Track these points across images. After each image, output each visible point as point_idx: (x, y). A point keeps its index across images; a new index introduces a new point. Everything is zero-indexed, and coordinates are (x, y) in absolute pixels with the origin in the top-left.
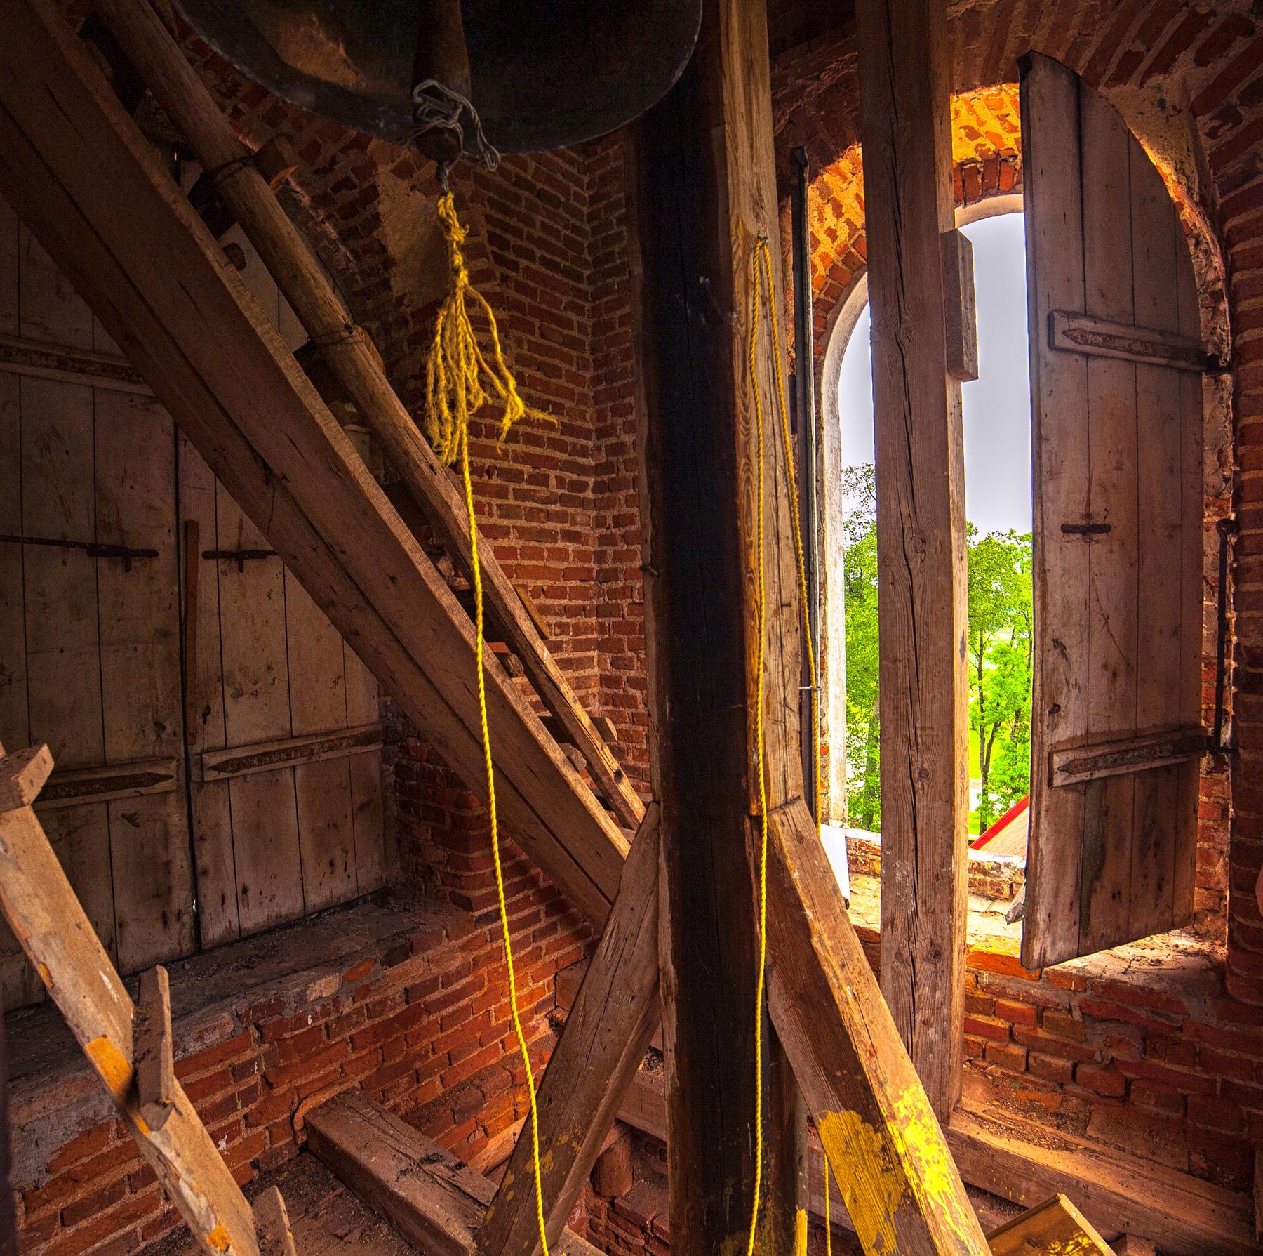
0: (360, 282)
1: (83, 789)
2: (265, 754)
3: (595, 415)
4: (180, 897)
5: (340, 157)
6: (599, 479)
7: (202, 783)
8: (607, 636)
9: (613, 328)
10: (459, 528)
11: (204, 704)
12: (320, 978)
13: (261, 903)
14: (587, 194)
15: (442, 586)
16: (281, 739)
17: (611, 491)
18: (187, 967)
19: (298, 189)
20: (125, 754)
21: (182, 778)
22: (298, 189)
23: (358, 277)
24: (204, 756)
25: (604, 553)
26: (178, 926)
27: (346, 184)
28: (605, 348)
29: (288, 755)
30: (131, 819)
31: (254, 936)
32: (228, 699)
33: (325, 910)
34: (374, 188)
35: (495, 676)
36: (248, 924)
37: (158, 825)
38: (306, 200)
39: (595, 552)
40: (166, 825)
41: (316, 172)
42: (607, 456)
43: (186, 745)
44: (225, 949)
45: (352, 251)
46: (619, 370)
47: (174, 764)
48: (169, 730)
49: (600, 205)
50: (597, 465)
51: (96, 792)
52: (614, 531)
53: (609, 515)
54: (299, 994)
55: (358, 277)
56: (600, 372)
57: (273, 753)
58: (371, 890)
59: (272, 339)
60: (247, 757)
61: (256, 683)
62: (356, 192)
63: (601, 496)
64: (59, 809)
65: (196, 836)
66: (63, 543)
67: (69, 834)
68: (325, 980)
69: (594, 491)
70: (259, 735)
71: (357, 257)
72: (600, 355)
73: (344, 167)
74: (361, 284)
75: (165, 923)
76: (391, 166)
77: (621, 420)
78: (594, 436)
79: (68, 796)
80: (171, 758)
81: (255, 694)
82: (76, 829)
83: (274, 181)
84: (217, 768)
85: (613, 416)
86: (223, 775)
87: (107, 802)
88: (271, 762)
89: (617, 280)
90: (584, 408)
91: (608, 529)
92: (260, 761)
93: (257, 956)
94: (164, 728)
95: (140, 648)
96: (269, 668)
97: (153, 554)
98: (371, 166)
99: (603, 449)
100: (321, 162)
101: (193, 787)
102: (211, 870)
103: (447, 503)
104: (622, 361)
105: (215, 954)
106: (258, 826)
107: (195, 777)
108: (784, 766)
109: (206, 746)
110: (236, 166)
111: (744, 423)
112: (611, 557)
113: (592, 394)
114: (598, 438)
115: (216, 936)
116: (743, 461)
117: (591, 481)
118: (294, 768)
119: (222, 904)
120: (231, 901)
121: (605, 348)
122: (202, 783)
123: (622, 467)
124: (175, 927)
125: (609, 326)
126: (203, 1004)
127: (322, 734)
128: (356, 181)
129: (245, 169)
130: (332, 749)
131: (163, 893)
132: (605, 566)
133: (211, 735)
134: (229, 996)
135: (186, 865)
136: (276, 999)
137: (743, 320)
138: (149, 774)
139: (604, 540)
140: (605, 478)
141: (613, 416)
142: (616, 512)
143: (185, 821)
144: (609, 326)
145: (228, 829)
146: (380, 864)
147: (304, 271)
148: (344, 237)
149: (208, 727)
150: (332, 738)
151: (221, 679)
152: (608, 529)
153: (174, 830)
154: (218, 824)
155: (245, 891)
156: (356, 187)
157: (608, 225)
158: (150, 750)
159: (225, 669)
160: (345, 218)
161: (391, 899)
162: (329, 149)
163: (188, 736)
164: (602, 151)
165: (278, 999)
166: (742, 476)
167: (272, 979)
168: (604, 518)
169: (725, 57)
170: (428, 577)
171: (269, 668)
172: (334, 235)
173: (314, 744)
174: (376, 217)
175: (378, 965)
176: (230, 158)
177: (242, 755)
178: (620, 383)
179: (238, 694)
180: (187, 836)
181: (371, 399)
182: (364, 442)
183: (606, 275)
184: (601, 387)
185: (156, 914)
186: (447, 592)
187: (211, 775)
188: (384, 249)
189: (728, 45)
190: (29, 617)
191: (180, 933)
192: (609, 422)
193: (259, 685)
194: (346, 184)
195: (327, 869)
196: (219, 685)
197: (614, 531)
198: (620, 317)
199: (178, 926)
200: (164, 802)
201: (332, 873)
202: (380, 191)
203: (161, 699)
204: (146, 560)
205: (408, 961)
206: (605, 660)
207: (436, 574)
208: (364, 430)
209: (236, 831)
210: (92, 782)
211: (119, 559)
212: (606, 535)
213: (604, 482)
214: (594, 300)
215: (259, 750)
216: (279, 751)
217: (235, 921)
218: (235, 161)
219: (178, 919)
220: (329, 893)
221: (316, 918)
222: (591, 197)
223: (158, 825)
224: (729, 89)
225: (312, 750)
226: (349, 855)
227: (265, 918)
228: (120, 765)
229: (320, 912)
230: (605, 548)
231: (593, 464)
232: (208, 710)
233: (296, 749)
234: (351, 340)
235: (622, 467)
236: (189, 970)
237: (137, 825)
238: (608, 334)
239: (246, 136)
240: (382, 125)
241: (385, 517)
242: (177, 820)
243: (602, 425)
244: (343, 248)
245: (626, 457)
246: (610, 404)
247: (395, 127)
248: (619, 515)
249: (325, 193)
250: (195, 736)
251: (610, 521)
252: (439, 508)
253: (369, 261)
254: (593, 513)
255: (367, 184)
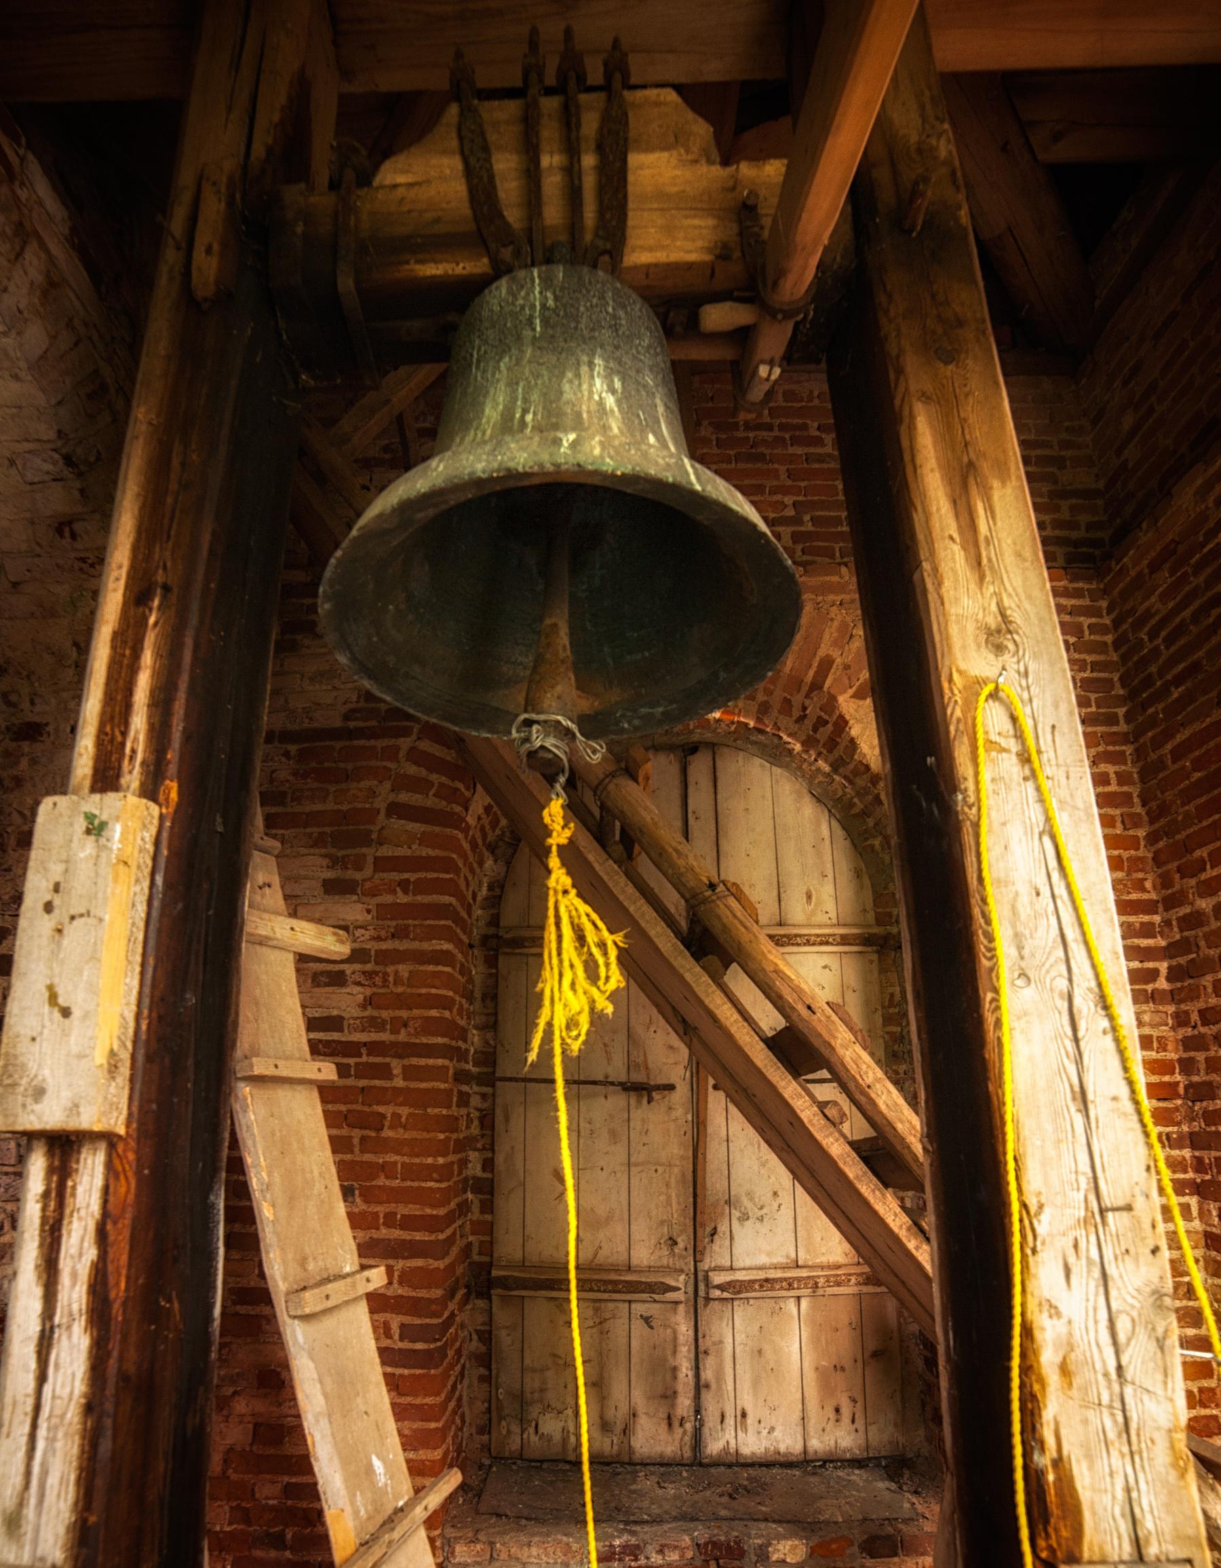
0: (859, 803)
1: (610, 1287)
2: (767, 1280)
3: (1159, 881)
4: (684, 1404)
5: (807, 702)
6: (1174, 963)
7: (708, 1299)
8: (1208, 1177)
9: (1165, 767)
10: (847, 1070)
11: (713, 1225)
12: (785, 1538)
13: (759, 1433)
14: (1107, 621)
15: (831, 1134)
16: (784, 1268)
17: (1192, 977)
18: (685, 1474)
19: (789, 740)
20: (645, 1263)
21: (691, 1289)
22: (789, 740)
23: (856, 800)
24: (710, 1274)
25: (1191, 1061)
26: (680, 1431)
27: (821, 722)
28: (1159, 795)
29: (790, 1285)
30: (647, 1320)
31: (752, 1465)
32: (735, 1223)
33: (831, 1461)
34: (841, 717)
35: (904, 1240)
36: (746, 1451)
37: (669, 1331)
38: (798, 747)
39: (1180, 1060)
40: (675, 1332)
41: (797, 721)
42: (1181, 931)
43: (695, 1262)
44: (723, 1468)
45: (845, 777)
46: (1180, 818)
47: (682, 1277)
48: (681, 1245)
49: (1125, 626)
50: (1170, 945)
51: (619, 1292)
52: (1203, 1030)
53: (1193, 1009)
54: (760, 1546)
55: (856, 800)
56: (1156, 826)
57: (775, 1280)
58: (883, 1453)
59: (643, 914)
60: (750, 1281)
61: (761, 1208)
62: (830, 727)
63: (1179, 985)
64: (595, 1301)
65: (702, 1348)
66: (606, 1083)
67: (601, 1323)
68: (790, 1543)
69: (1168, 979)
70: (763, 1260)
71: (851, 782)
72: (1154, 805)
73: (813, 711)
74: (859, 806)
75: (670, 1425)
76: (851, 692)
77: (1193, 882)
78: (1161, 908)
79: (599, 1291)
80: (682, 1271)
81: (761, 1219)
82: (606, 1320)
83: (640, 779)
84: (721, 1287)
85: (1182, 878)
86: (726, 1295)
87: (630, 1302)
88: (772, 1289)
89: (1161, 706)
90: (1140, 875)
91: (1194, 1027)
92: (761, 1286)
93: (745, 1488)
94: (676, 1243)
95: (660, 1169)
96: (775, 1194)
97: (671, 1087)
98: (833, 699)
99: (1174, 923)
100: (796, 713)
101: (701, 1302)
102: (713, 1385)
103: (830, 1045)
104: (1183, 804)
105: (713, 1470)
106: (760, 1352)
107: (702, 1293)
108: (1128, 1490)
109: (713, 1265)
110: (607, 780)
111: (985, 942)
112: (1202, 1066)
113: (1150, 855)
114: (1166, 910)
115: (715, 1452)
116: (989, 996)
117: (1163, 966)
118: (799, 1298)
119: (722, 1422)
120: (730, 1421)
121: (1159, 795)
122: (708, 1299)
123: (1202, 943)
124: (678, 1431)
125: (1160, 765)
126: (675, 1519)
127: (830, 1267)
128: (826, 717)
129: (615, 781)
130: (838, 1284)
131: (669, 1396)
132: (1196, 1079)
133: (718, 1255)
134: (697, 1520)
135: (690, 1374)
136: (735, 1542)
137: (972, 799)
138: (662, 1283)
139: (1188, 1043)
140: (1182, 960)
141: (1182, 878)
142: (1201, 1005)
143: (691, 1333)
144: (1160, 765)
145: (729, 1349)
146: (896, 1425)
147: (667, 847)
148: (835, 767)
149: (716, 1247)
150: (839, 1272)
151: (728, 1202)
152: (1194, 1027)
153: (681, 1339)
154: (721, 1342)
155: (744, 1415)
156: (827, 722)
157: (1140, 644)
158: (665, 1261)
159: (732, 1193)
160: (830, 751)
161: (907, 1474)
162: (797, 699)
163: (697, 1252)
164: (1117, 564)
165: (737, 1543)
166: (990, 1019)
167: (741, 1519)
168: (1187, 1013)
169: (912, 486)
170: (813, 1125)
171: (775, 1194)
172: (827, 769)
173: (818, 1277)
174: (852, 740)
175: (855, 1549)
176: (602, 776)
177: (747, 1278)
178: (1184, 834)
179: (744, 1218)
180: (693, 1347)
181: (739, 949)
182: (871, 962)
183: (1144, 706)
184: (1161, 844)
185: (662, 1415)
186: (837, 1140)
187: (717, 1293)
188: (867, 767)
189: (915, 471)
190: (582, 1141)
191: (682, 1439)
192: (1177, 887)
193: (765, 1211)
194: (821, 722)
195: (832, 1415)
196: (727, 1208)
197: (1203, 1030)
198: (1171, 751)
199: (680, 1431)
200: (675, 1311)
201: (837, 1421)
202: (847, 717)
203: (675, 1216)
204: (666, 1092)
205: (896, 1559)
206: (1209, 1211)
207: (823, 1121)
208: (869, 949)
209: (737, 1351)
210: (616, 1283)
211: (645, 1093)
212: (1193, 1037)
213: (1180, 965)
214: (1136, 740)
215: (761, 1275)
216: (781, 1280)
217: (732, 1443)
218: (607, 776)
219: (681, 1425)
220: (832, 1443)
221: (820, 1466)
222: (1113, 621)
223: (669, 1331)
224: (923, 519)
225: (816, 1283)
226: (858, 1404)
227: (763, 1450)
228: (640, 1272)
229: (825, 1462)
230: (1192, 1054)
231: (1163, 943)
232: (714, 1233)
233: (799, 1279)
234: (714, 897)
235: (1202, 943)
236: (684, 1478)
237: (652, 1328)
238: (1161, 776)
239: (739, 715)
240: (626, 725)
241: (759, 1064)
242: (684, 1329)
243: (1170, 891)
244: (837, 778)
245: (1206, 929)
246: (1176, 864)
247: (636, 722)
248: (1207, 1009)
249: (809, 736)
250: (702, 1253)
251: (1195, 1017)
252: (823, 1050)
253: (861, 782)
254: (1171, 1009)
255: (835, 718)
